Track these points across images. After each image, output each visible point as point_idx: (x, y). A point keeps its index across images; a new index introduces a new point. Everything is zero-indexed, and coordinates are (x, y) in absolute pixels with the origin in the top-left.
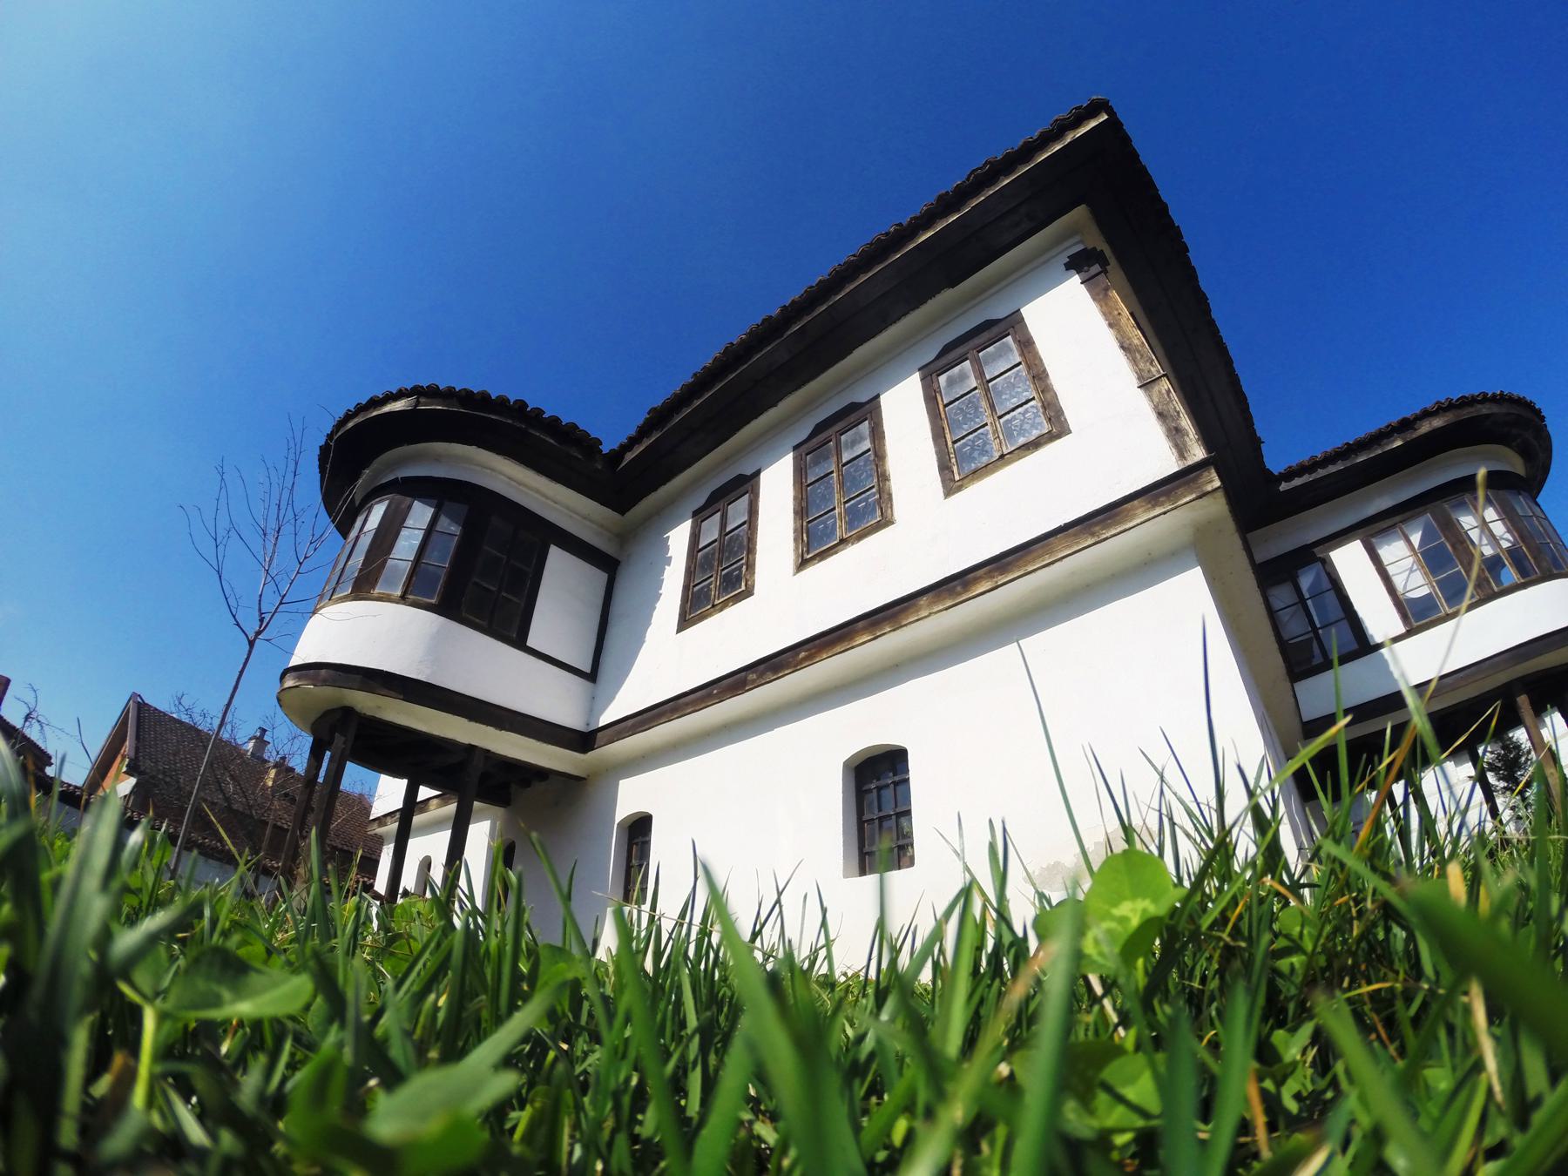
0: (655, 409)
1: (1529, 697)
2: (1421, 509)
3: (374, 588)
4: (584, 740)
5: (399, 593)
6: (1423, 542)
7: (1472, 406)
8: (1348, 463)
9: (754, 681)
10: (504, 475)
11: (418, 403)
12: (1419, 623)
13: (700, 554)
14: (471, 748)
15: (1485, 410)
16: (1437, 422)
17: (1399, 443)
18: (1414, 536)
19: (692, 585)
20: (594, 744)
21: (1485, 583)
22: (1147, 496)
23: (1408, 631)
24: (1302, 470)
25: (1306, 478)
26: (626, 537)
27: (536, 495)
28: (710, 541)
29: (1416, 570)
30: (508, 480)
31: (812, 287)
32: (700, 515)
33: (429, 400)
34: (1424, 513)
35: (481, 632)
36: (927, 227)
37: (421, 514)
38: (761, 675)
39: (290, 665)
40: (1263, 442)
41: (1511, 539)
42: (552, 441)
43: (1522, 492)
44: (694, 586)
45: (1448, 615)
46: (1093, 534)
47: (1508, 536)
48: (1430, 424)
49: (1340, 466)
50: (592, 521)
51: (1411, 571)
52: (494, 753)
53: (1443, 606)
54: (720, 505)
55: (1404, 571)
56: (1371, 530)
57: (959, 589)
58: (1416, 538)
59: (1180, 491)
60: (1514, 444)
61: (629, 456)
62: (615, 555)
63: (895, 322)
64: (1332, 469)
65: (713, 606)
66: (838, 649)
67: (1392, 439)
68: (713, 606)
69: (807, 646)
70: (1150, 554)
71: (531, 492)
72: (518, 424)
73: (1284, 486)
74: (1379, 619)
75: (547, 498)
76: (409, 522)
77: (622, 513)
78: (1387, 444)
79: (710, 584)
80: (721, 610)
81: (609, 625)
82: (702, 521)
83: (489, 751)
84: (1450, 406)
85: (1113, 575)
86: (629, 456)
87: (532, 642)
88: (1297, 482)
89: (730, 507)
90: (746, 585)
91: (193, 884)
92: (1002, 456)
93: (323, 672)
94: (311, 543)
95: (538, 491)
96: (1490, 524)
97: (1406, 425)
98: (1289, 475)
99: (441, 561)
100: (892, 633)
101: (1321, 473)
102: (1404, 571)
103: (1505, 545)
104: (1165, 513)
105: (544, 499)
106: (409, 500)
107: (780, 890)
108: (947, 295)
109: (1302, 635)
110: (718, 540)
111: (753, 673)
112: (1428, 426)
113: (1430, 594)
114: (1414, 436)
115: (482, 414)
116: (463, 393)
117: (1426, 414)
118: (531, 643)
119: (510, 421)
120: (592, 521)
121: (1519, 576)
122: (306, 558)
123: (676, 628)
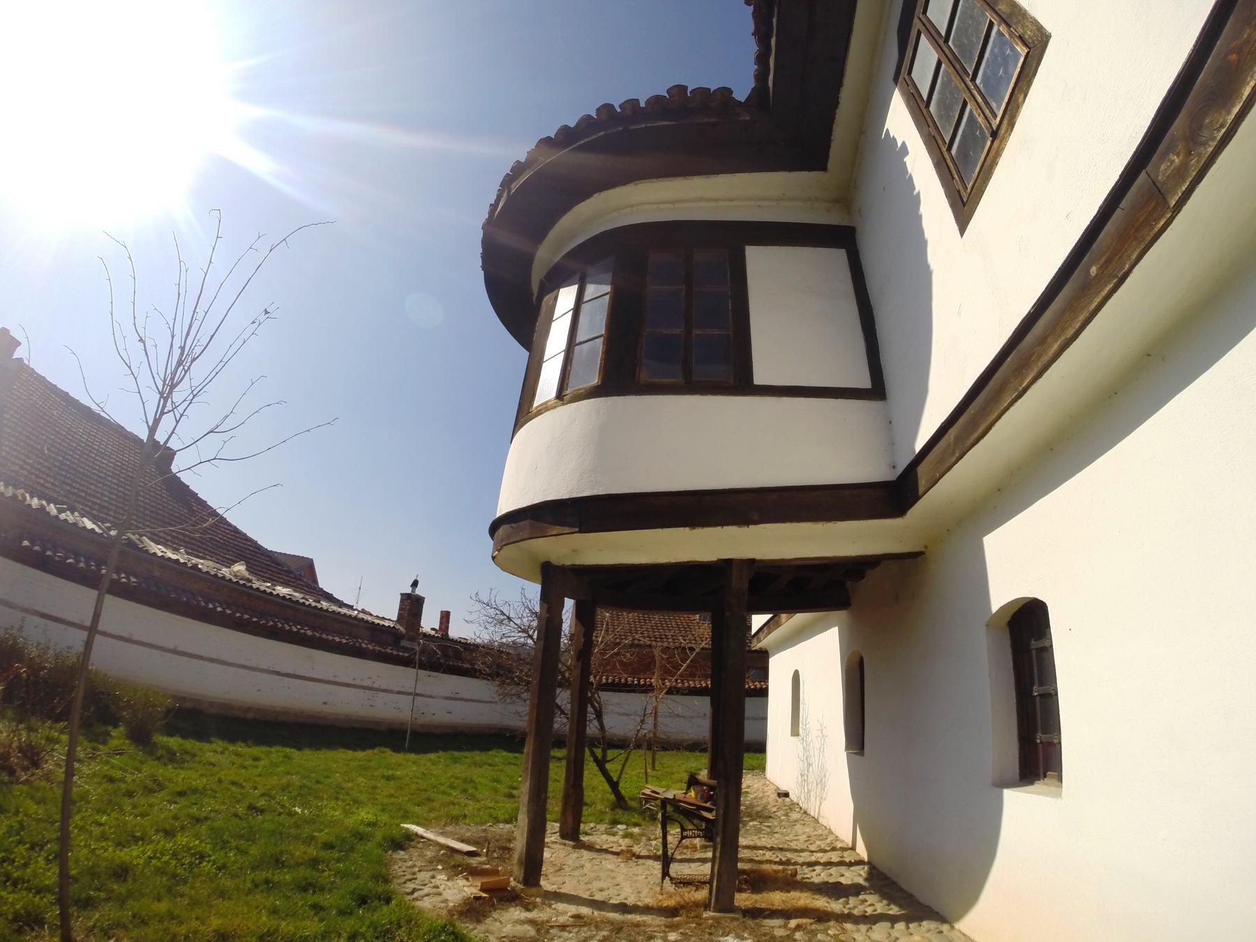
9: (1180, 173)
13: (932, 108)
19: (944, 149)
26: (847, 197)
28: (932, 72)
35: (702, 394)
38: (1193, 139)
39: (498, 515)
44: (949, 149)
52: (762, 561)
54: (917, 24)
62: (845, 223)
68: (994, 134)
75: (716, 200)
77: (823, 168)
79: (972, 118)
80: (1012, 125)
82: (910, 73)
83: (753, 561)
87: (760, 377)
89: (928, 14)
90: (1025, 44)
91: (73, 910)
105: (713, 204)
107: (178, 419)
110: (944, 60)
111: (1164, 156)
118: (759, 379)
123: (956, 228)
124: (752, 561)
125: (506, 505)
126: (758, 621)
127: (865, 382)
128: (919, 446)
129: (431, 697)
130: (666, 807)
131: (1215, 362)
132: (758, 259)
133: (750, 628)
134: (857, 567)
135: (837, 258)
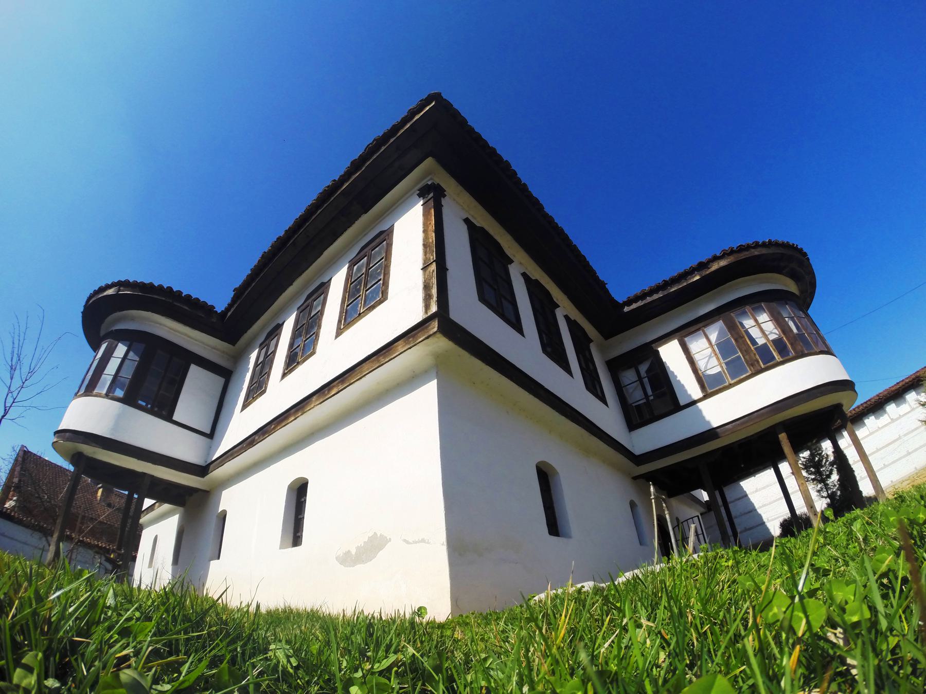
0: (237, 288)
1: (787, 434)
2: (717, 317)
3: (94, 390)
4: (202, 470)
5: (104, 392)
6: (718, 339)
7: (748, 251)
8: (666, 293)
10: (167, 327)
11: (119, 290)
12: (711, 391)
14: (144, 474)
15: (756, 252)
16: (723, 263)
17: (697, 278)
18: (713, 335)
20: (208, 471)
21: (756, 363)
22: (404, 339)
23: (704, 396)
24: (636, 299)
25: (640, 303)
27: (185, 337)
29: (713, 357)
30: (168, 329)
31: (297, 219)
32: (261, 346)
33: (126, 289)
34: (718, 320)
36: (347, 181)
37: (121, 349)
40: (607, 284)
41: (778, 333)
42: (187, 308)
43: (788, 302)
45: (730, 384)
46: (379, 361)
47: (776, 331)
48: (718, 264)
49: (660, 295)
50: (217, 350)
51: (710, 357)
53: (727, 379)
55: (706, 357)
56: (683, 333)
57: (326, 392)
58: (713, 337)
59: (419, 335)
60: (784, 271)
61: (229, 314)
63: (341, 235)
64: (655, 297)
65: (253, 398)
66: (283, 424)
67: (694, 275)
68: (253, 398)
69: (274, 422)
70: (414, 372)
71: (182, 336)
72: (168, 300)
73: (626, 309)
74: (690, 387)
76: (115, 354)
77: (234, 344)
78: (690, 279)
81: (223, 407)
83: (153, 476)
84: (732, 252)
85: (398, 384)
86: (229, 314)
88: (634, 306)
92: (360, 314)
93: (67, 434)
94: (29, 373)
95: (186, 335)
96: (761, 325)
97: (702, 266)
98: (629, 302)
99: (128, 374)
100: (302, 416)
101: (649, 299)
102: (706, 357)
103: (772, 337)
104: (410, 348)
106: (116, 342)
108: (364, 218)
109: (641, 400)
112: (717, 265)
113: (720, 372)
114: (707, 273)
115: (149, 295)
116: (141, 284)
117: (715, 258)
118: (175, 418)
119: (164, 299)
120: (217, 350)
121: (779, 357)
122: (26, 380)
124: (153, 476)
125: (62, 427)
126: (148, 502)
127: (208, 431)
128: (214, 459)
129: (12, 539)
130: (355, 677)
131: (567, 356)
132: (194, 371)
133: (142, 508)
134: (191, 491)
135: (220, 381)
